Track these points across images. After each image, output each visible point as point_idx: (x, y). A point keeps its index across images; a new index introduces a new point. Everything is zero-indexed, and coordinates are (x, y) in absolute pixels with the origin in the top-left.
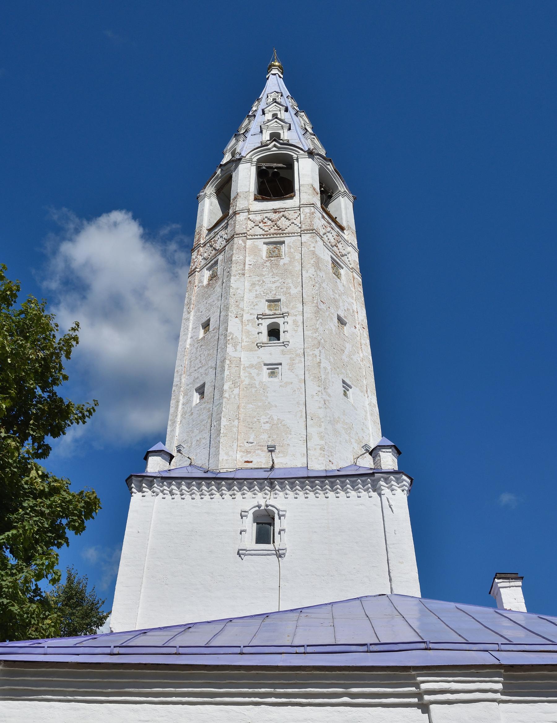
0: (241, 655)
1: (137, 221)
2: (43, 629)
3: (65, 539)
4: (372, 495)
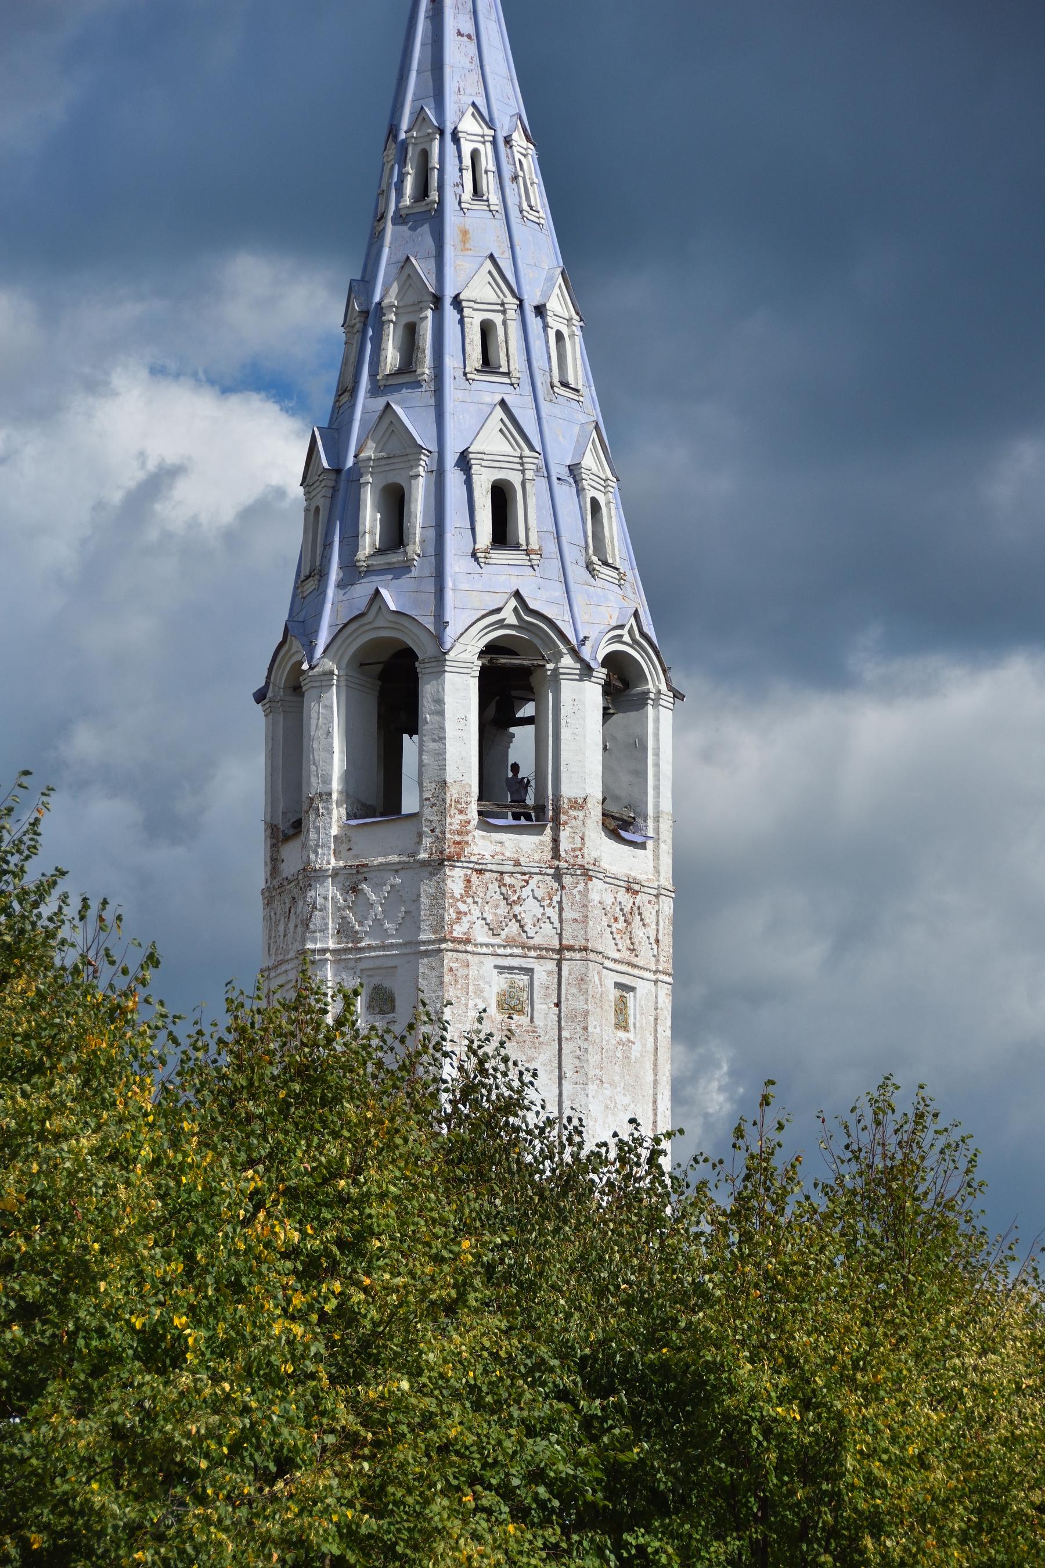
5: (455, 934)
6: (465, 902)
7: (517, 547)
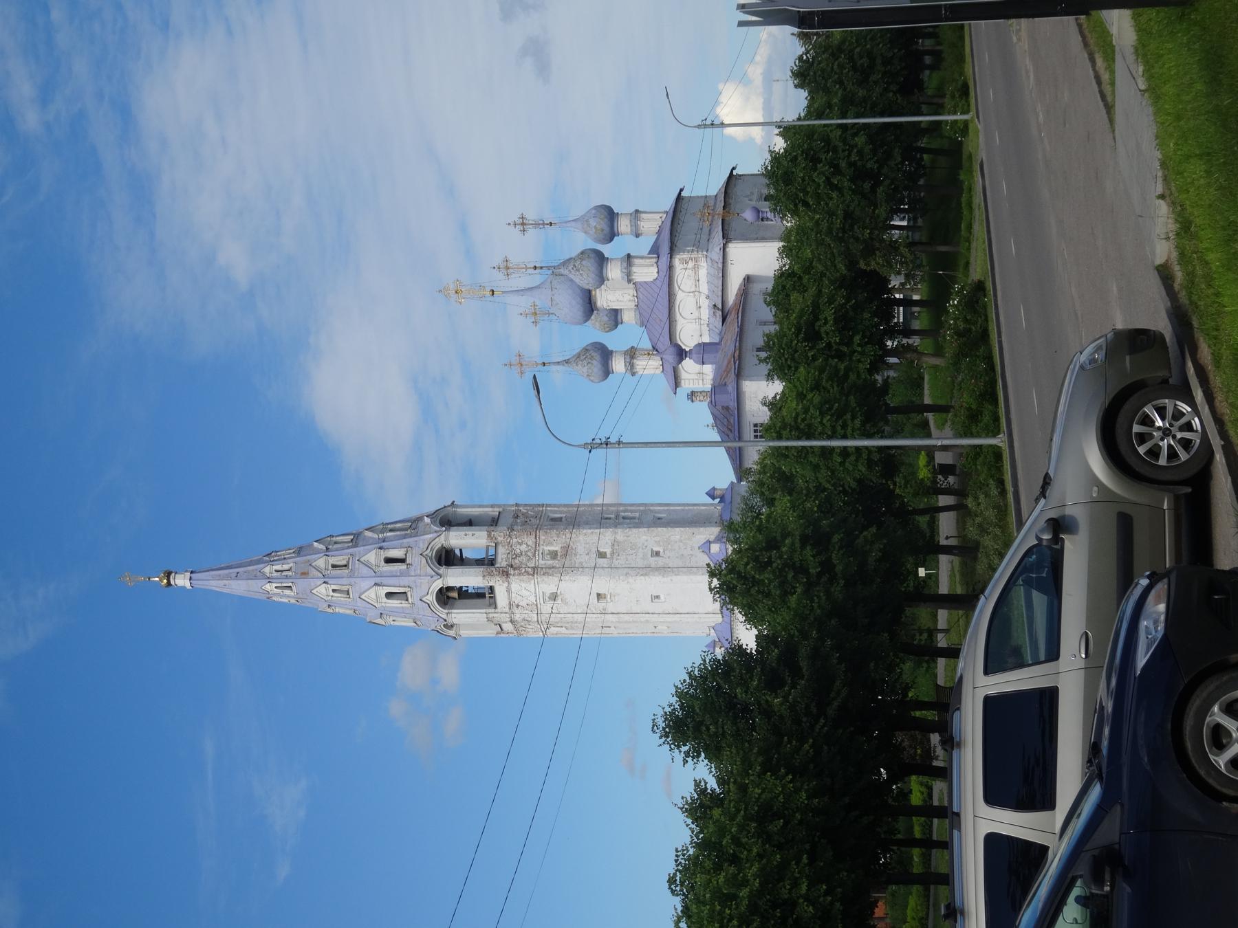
0: (1077, 30)
4: (455, 621)
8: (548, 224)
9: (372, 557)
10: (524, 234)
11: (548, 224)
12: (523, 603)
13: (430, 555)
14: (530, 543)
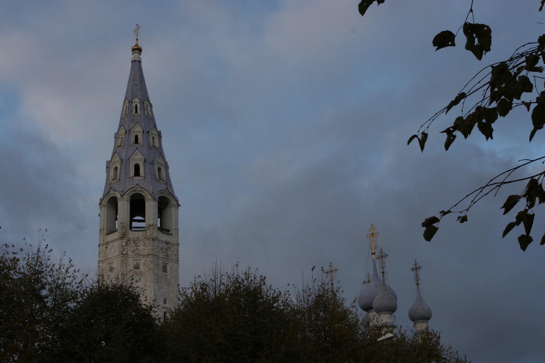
1: (537, 130)
2: (56, 315)
3: (394, 343)
5: (123, 253)
6: (126, 247)
7: (140, 176)
8: (417, 282)
9: (138, 158)
10: (411, 270)
11: (417, 282)
12: (108, 251)
13: (138, 190)
14: (145, 251)
